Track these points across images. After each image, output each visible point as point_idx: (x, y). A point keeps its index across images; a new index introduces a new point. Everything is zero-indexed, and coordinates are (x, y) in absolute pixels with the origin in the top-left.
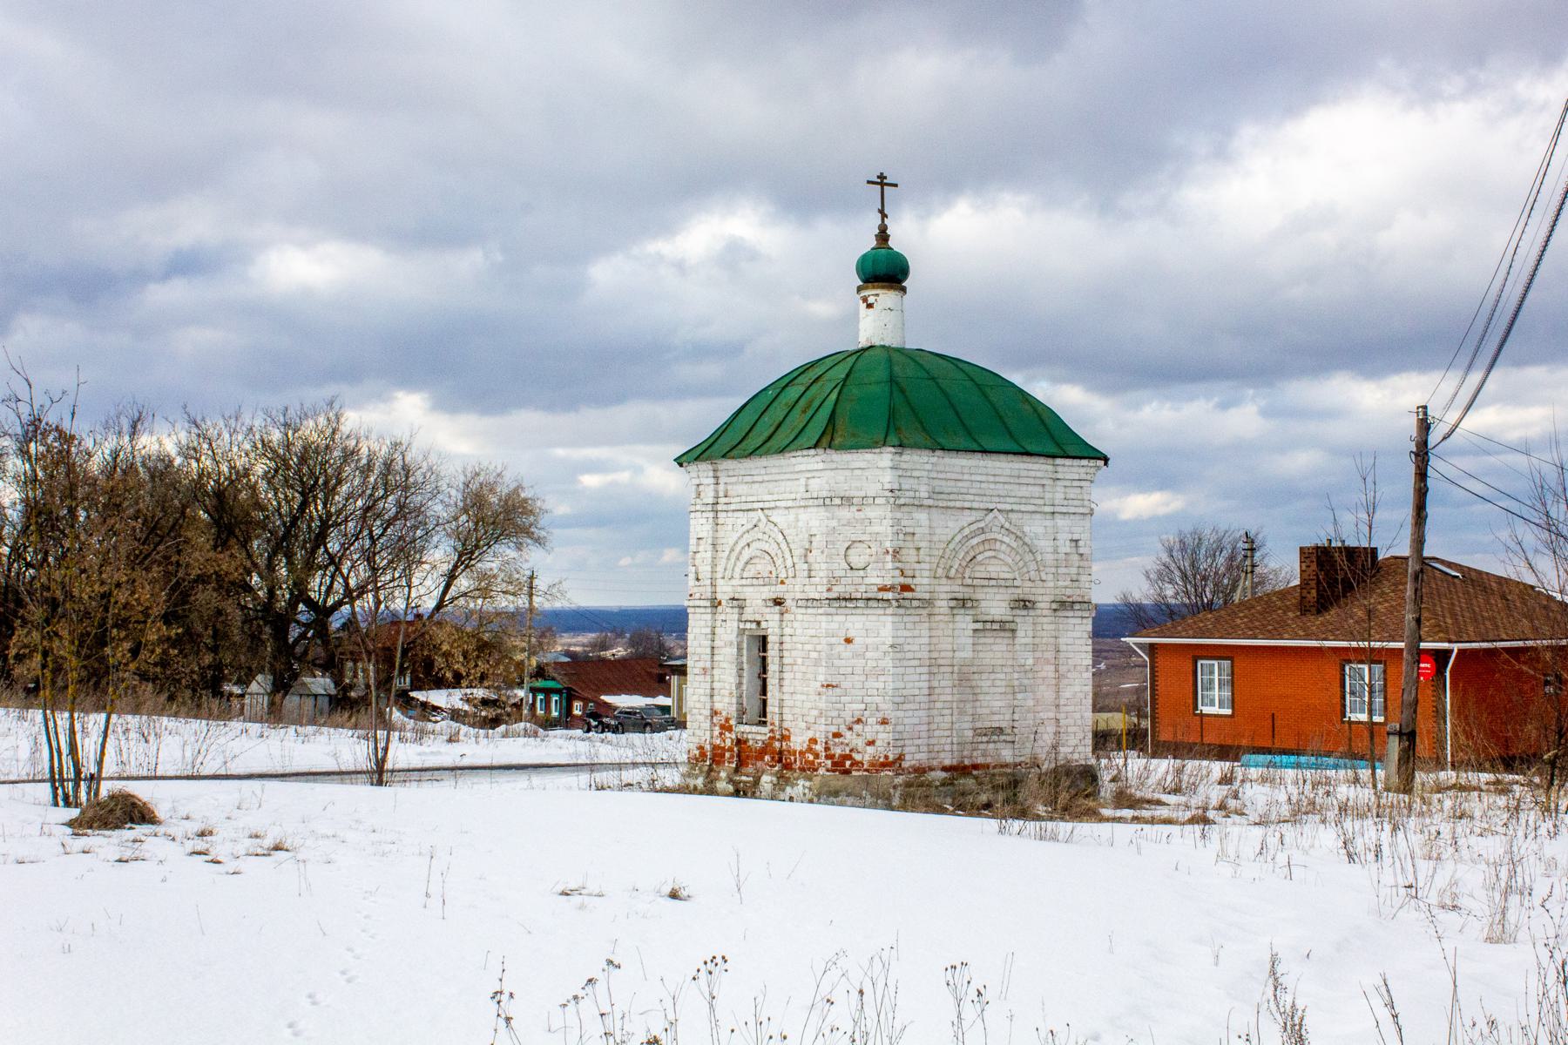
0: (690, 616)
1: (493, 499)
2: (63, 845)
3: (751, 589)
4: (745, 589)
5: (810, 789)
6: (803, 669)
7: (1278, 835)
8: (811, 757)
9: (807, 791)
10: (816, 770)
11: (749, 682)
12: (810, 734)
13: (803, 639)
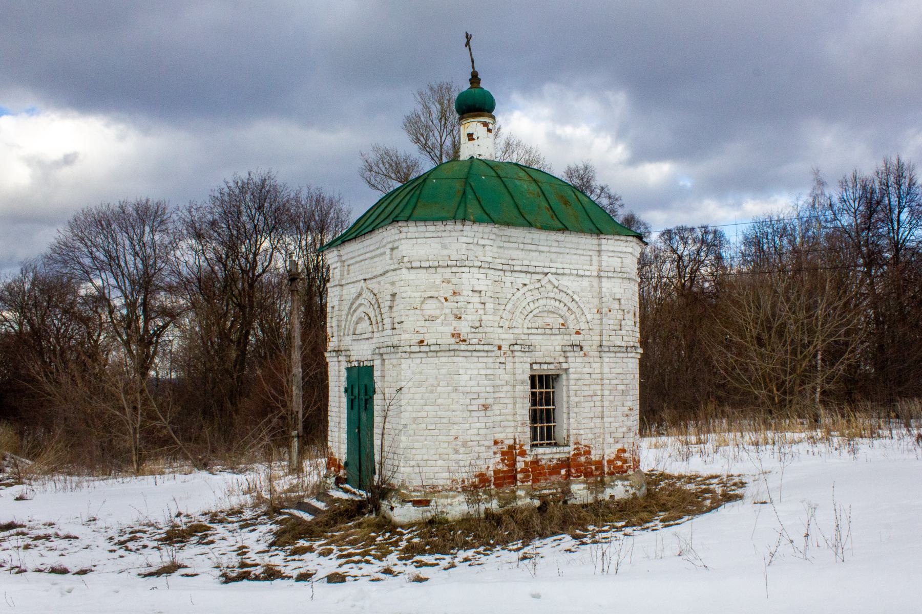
0: (330, 364)
1: (846, 220)
2: (83, 572)
3: (540, 337)
4: (531, 337)
5: (632, 486)
6: (611, 398)
7: (600, 553)
8: (619, 463)
9: (628, 488)
10: (625, 472)
11: (562, 406)
12: (619, 446)
13: (610, 376)
